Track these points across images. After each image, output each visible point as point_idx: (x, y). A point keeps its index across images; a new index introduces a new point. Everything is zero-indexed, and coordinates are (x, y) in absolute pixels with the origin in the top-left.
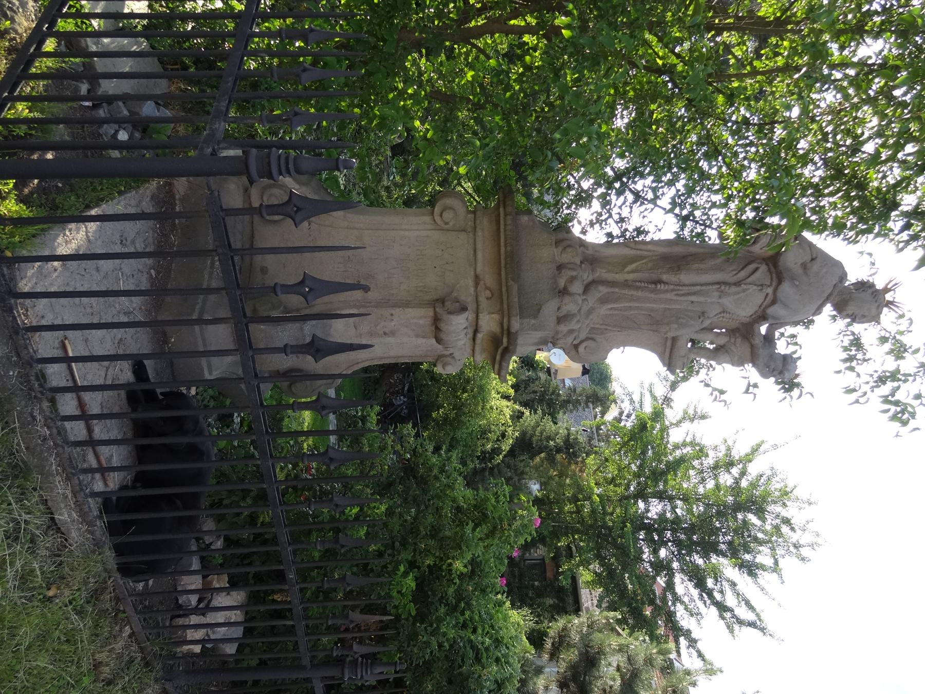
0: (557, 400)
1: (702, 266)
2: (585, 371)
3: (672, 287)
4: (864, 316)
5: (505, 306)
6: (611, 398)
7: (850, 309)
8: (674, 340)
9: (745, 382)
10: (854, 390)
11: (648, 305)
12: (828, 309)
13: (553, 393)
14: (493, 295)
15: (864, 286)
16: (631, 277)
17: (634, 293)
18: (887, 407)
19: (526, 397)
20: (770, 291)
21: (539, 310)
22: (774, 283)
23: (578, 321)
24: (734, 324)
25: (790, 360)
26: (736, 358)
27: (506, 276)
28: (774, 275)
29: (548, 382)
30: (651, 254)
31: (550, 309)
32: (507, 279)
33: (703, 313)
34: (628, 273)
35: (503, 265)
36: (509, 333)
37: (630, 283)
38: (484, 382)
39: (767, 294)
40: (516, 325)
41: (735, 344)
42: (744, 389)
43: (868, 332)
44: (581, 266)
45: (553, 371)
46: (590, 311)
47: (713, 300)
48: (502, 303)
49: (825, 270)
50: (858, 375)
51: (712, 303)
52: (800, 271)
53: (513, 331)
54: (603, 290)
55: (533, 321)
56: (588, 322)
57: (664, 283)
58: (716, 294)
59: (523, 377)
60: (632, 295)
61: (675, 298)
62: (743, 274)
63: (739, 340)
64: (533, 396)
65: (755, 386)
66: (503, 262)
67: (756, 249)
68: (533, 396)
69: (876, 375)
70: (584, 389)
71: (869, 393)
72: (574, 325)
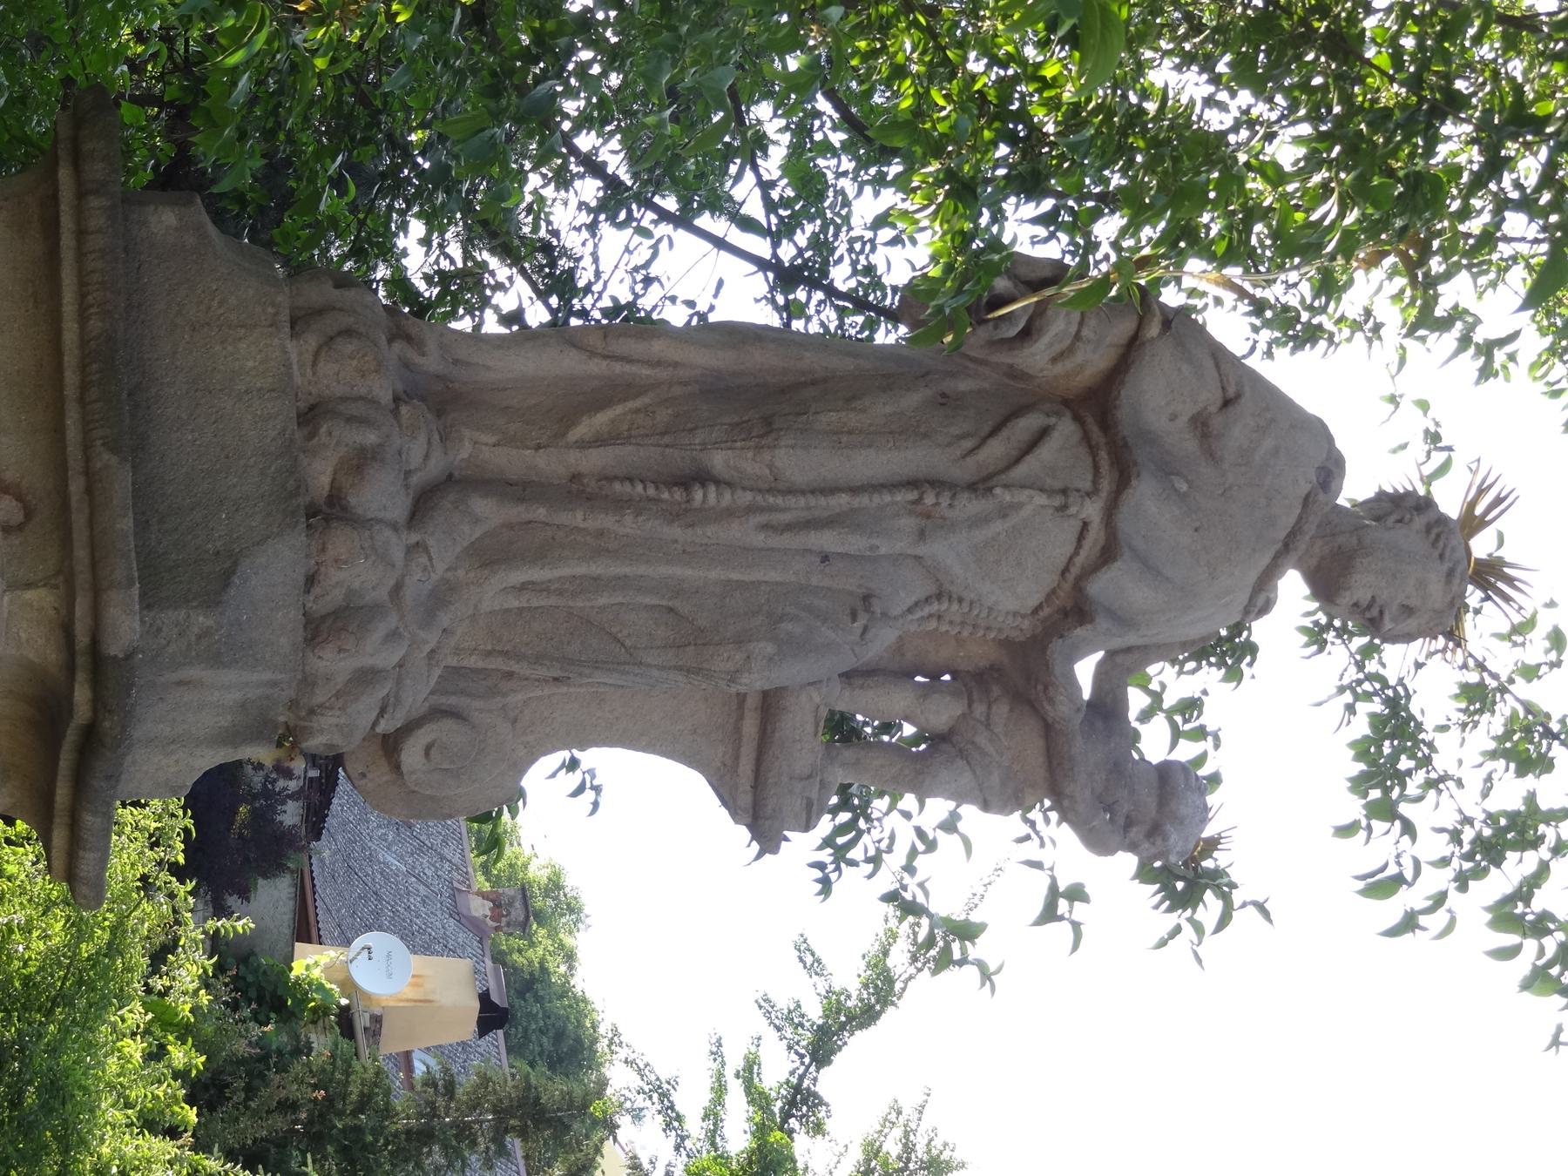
0: (377, 1131)
1: (853, 419)
2: (491, 1017)
3: (747, 498)
4: (1408, 611)
5: (81, 553)
6: (596, 1108)
7: (1362, 586)
8: (770, 704)
9: (1038, 886)
10: (1398, 881)
11: (663, 570)
12: (1292, 588)
13: (364, 1103)
14: (29, 513)
15: (1403, 509)
16: (594, 461)
17: (605, 521)
18: (1511, 939)
19: (252, 1129)
20: (1093, 510)
21: (226, 578)
22: (1106, 485)
23: (393, 635)
24: (980, 653)
25: (1180, 780)
26: (995, 779)
27: (86, 432)
28: (1103, 455)
29: (343, 1063)
30: (664, 374)
31: (273, 571)
32: (87, 447)
33: (867, 598)
34: (583, 445)
35: (71, 390)
36: (98, 661)
37: (592, 485)
38: (66, 1059)
39: (1085, 525)
40: (125, 626)
41: (988, 725)
42: (1038, 907)
43: (1428, 677)
44: (395, 412)
45: (361, 1022)
46: (440, 598)
47: (901, 546)
48: (66, 542)
49: (1268, 443)
50: (1409, 829)
51: (896, 559)
52: (1190, 445)
53: (114, 649)
54: (488, 511)
55: (202, 620)
56: (431, 638)
57: (718, 482)
58: (908, 523)
59: (241, 1048)
60: (601, 533)
61: (759, 539)
62: (996, 450)
63: (1002, 710)
64: (279, 1123)
65: (1077, 894)
66: (71, 378)
67: (1036, 357)
68: (279, 1123)
69: (1468, 835)
70: (485, 1080)
71: (1454, 898)
72: (374, 651)
